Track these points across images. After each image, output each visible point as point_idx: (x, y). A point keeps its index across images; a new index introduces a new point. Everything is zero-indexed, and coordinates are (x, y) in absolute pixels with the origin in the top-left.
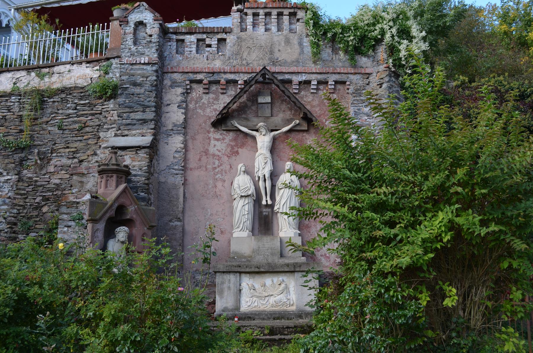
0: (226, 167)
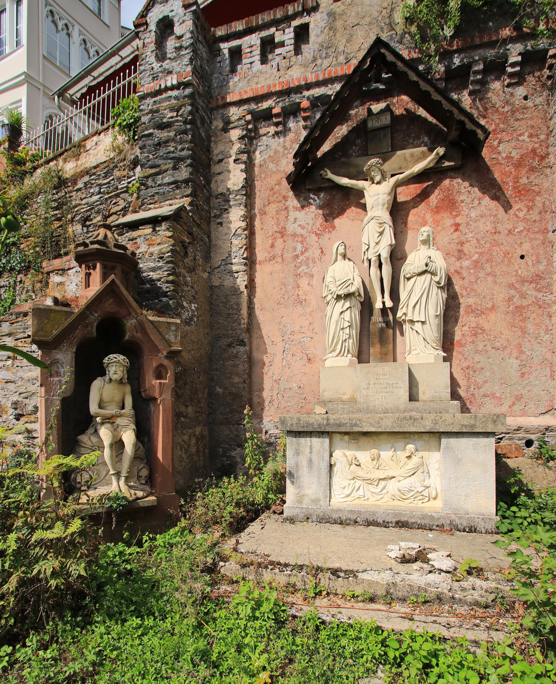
0: (313, 253)
